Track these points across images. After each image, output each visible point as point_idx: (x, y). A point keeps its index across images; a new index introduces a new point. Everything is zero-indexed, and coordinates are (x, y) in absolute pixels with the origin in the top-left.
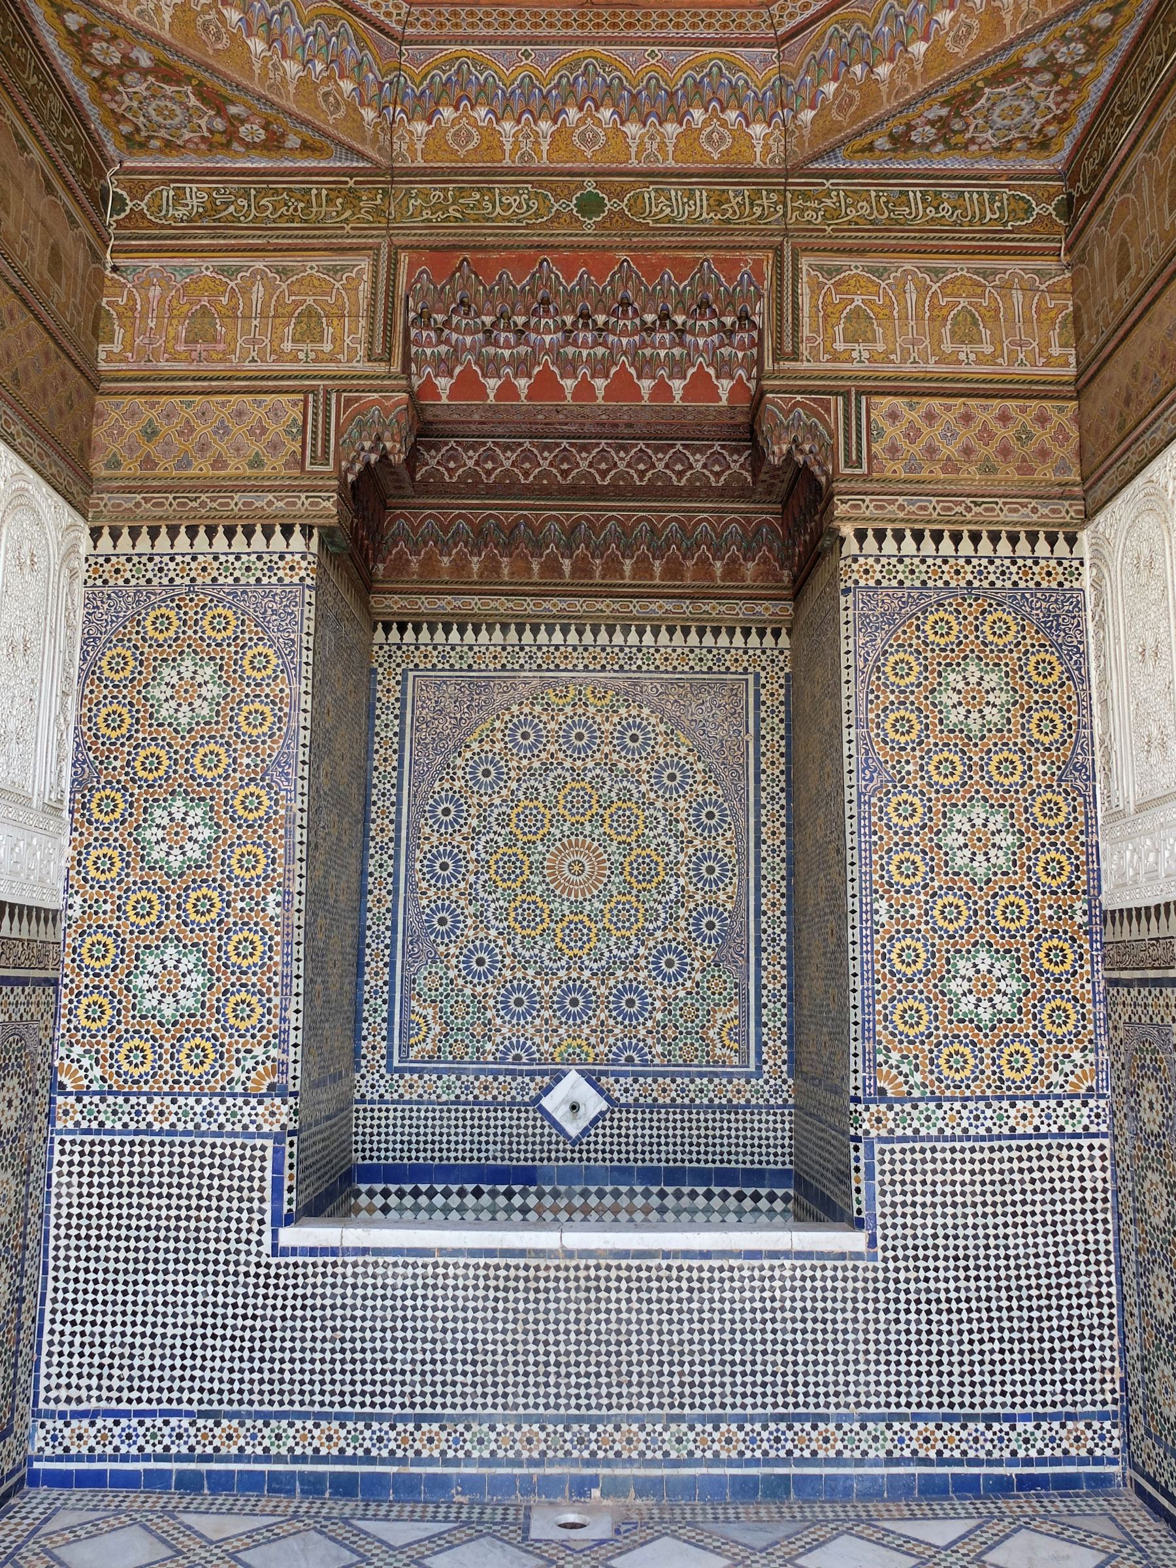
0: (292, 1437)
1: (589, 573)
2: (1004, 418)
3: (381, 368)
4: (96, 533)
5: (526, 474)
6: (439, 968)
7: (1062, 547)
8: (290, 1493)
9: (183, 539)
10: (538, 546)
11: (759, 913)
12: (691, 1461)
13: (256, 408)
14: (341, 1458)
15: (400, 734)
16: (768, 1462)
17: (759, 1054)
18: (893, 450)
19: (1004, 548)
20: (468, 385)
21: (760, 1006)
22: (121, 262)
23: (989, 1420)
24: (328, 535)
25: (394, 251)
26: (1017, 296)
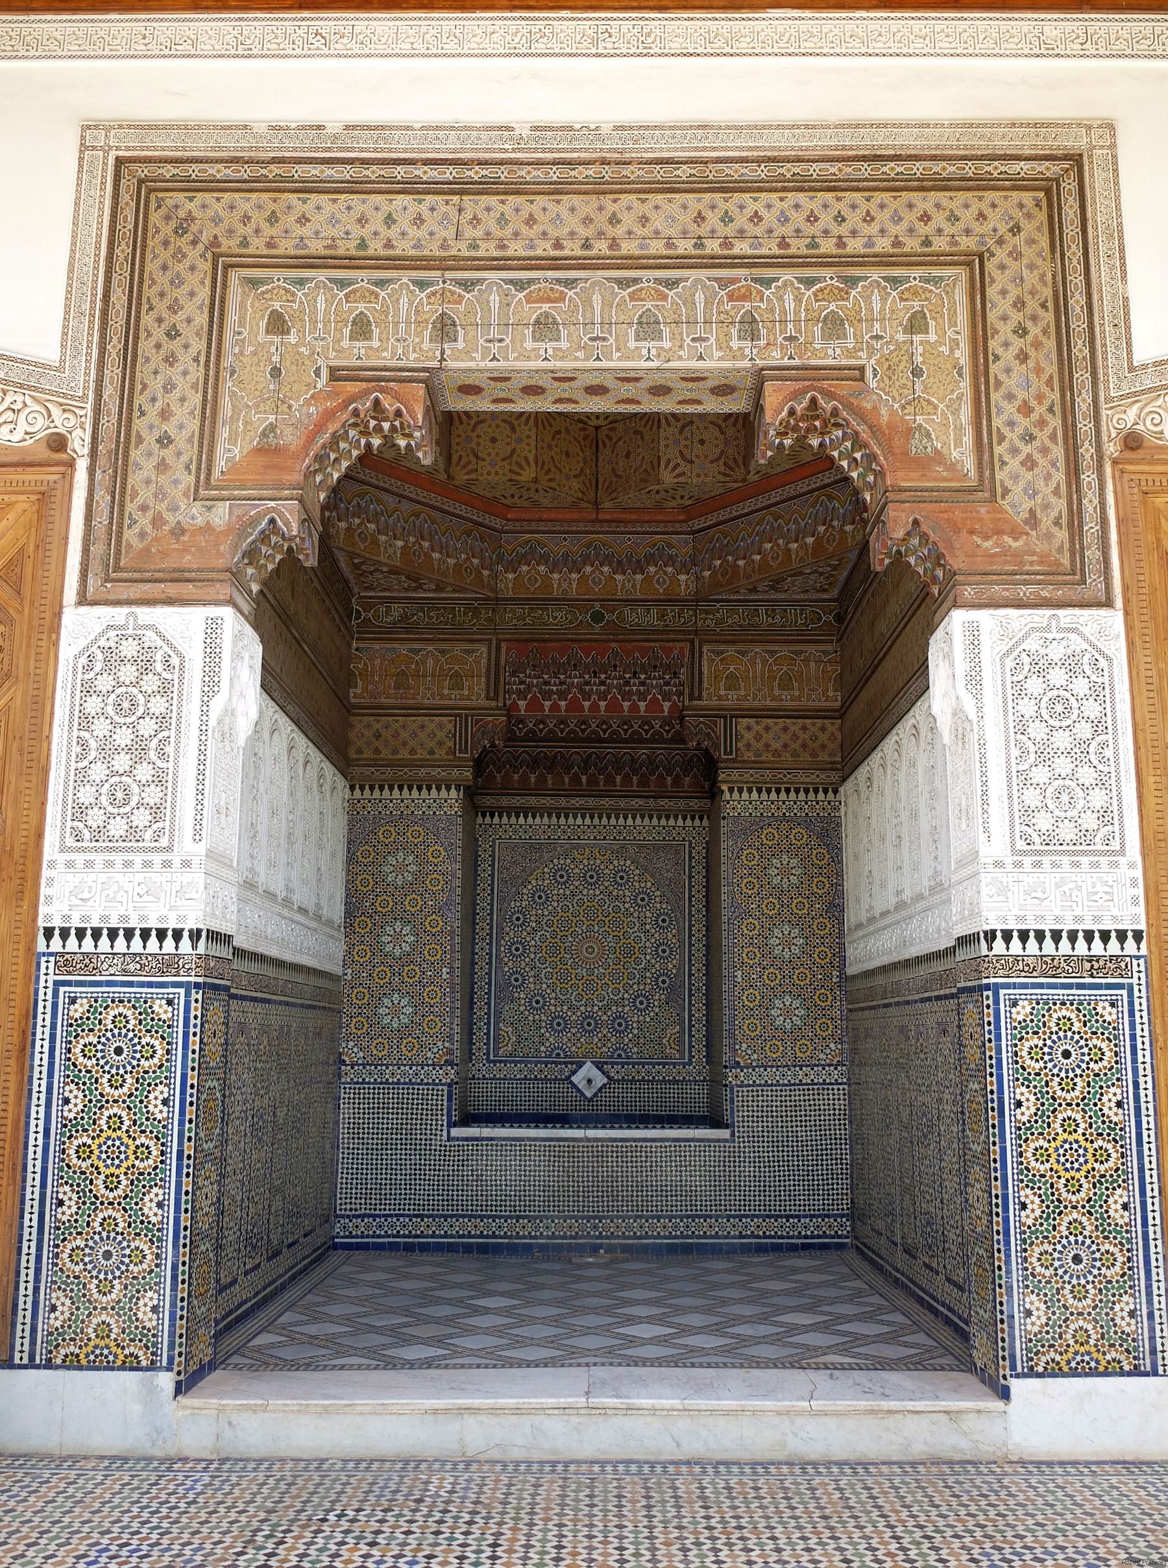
0: (457, 1226)
1: (597, 783)
2: (804, 728)
3: (493, 704)
4: (352, 788)
5: (562, 731)
6: (514, 1006)
7: (830, 795)
8: (457, 1252)
9: (396, 791)
10: (568, 769)
11: (690, 975)
12: (647, 1237)
13: (431, 724)
14: (481, 1236)
15: (492, 875)
16: (683, 1237)
17: (690, 1052)
18: (748, 745)
19: (802, 796)
20: (534, 705)
21: (691, 1026)
22: (361, 645)
23: (788, 1217)
24: (467, 788)
25: (499, 641)
26: (812, 664)
